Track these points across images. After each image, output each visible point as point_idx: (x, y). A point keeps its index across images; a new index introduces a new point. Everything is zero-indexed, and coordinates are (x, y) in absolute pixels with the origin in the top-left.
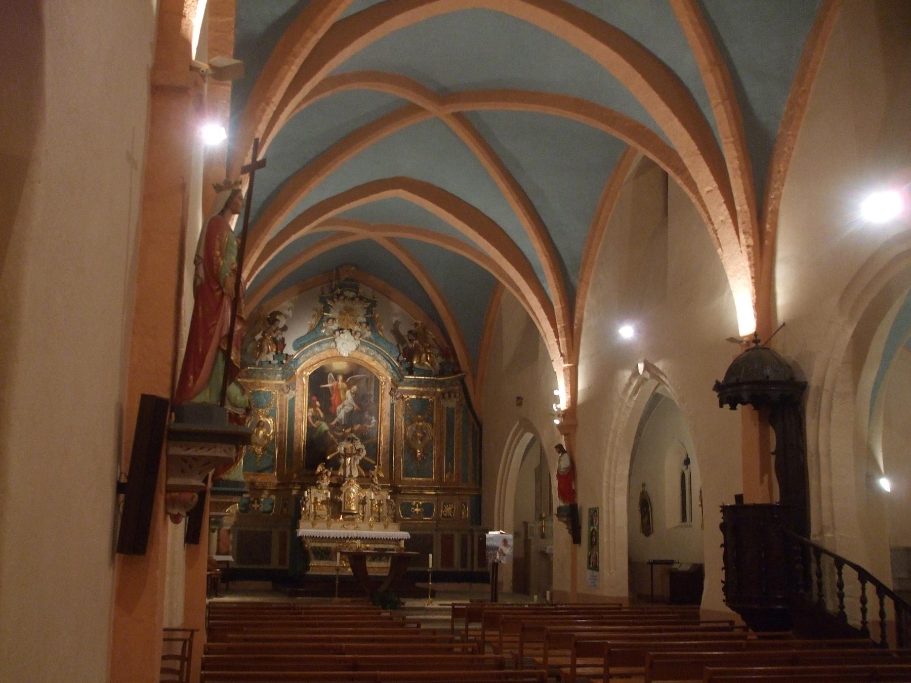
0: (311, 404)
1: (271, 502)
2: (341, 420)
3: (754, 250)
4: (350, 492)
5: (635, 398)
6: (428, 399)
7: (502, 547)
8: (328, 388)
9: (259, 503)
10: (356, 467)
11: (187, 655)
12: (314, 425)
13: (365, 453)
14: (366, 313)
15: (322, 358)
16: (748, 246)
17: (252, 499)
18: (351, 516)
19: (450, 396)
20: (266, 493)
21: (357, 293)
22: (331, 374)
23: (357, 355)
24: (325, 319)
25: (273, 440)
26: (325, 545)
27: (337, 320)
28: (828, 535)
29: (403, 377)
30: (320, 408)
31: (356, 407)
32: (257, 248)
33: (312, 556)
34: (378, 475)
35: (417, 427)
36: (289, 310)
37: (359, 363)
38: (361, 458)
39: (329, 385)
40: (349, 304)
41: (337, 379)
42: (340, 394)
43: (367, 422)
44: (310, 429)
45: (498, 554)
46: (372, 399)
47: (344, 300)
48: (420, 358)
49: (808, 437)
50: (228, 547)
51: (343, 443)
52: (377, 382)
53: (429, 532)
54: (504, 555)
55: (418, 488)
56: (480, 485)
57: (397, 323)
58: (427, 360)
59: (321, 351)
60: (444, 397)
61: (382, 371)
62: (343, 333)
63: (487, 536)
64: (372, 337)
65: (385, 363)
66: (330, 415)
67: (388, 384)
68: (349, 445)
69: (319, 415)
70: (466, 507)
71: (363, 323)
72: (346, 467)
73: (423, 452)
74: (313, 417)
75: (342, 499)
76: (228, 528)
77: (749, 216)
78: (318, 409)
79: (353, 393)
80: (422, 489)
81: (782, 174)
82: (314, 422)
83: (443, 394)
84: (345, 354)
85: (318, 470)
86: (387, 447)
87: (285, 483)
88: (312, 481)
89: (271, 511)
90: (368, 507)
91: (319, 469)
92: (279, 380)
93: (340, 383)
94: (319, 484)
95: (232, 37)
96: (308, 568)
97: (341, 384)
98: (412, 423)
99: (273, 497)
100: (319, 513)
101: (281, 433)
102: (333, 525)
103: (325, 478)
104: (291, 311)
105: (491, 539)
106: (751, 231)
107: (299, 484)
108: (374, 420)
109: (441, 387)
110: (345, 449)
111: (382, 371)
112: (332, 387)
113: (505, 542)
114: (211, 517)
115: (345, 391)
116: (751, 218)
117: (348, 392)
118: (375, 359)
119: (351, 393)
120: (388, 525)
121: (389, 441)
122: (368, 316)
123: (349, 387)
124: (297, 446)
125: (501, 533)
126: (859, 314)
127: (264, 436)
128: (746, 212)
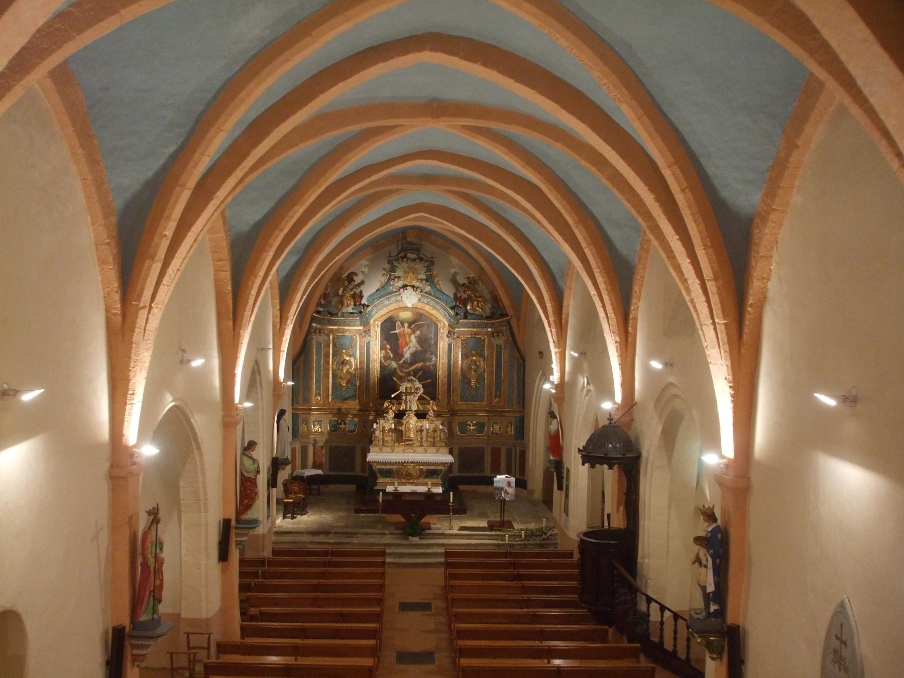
0: (383, 348)
1: (354, 423)
2: (407, 359)
3: (620, 345)
4: (409, 424)
5: (587, 398)
6: (481, 338)
7: (506, 488)
8: (396, 333)
9: (345, 424)
10: (415, 402)
11: (192, 667)
12: (386, 364)
13: (422, 390)
14: (425, 271)
15: (391, 310)
16: (616, 342)
17: (339, 421)
18: (410, 442)
19: (498, 335)
20: (350, 416)
21: (418, 255)
22: (399, 322)
23: (420, 305)
24: (392, 278)
25: (355, 374)
26: (388, 467)
27: (402, 278)
28: (646, 560)
29: (459, 321)
30: (390, 350)
31: (419, 348)
32: (305, 277)
33: (379, 475)
34: (433, 409)
35: (472, 360)
36: (365, 267)
37: (421, 312)
38: (419, 395)
39: (397, 331)
40: (412, 264)
41: (403, 326)
42: (406, 338)
43: (428, 360)
44: (382, 367)
45: (503, 493)
46: (432, 342)
47: (407, 261)
48: (473, 304)
49: (640, 490)
50: (322, 459)
51: (404, 383)
52: (437, 326)
53: (482, 446)
54: (508, 493)
55: (472, 411)
56: (524, 408)
57: (455, 274)
58: (478, 307)
59: (391, 304)
60: (493, 336)
61: (441, 317)
62: (406, 289)
63: (495, 479)
64: (431, 291)
65: (442, 311)
66: (398, 355)
67: (445, 328)
68: (409, 385)
69: (390, 356)
70: (511, 426)
71: (424, 279)
72: (407, 402)
73: (477, 382)
74: (385, 358)
75: (403, 429)
76: (322, 444)
77: (616, 321)
78: (389, 351)
79: (417, 337)
80: (475, 411)
81: (638, 293)
82: (386, 362)
83: (493, 333)
84: (409, 305)
85: (385, 406)
86: (446, 380)
87: (364, 410)
88: (381, 413)
89: (355, 430)
90: (425, 433)
91: (386, 404)
92: (358, 326)
93: (406, 329)
94: (385, 416)
95: (225, 244)
96: (376, 484)
97: (407, 330)
98: (467, 357)
99: (356, 420)
100: (386, 438)
101: (361, 369)
102: (396, 449)
103: (391, 412)
104: (367, 268)
105: (498, 481)
106: (617, 332)
107: (374, 411)
108: (434, 359)
109: (491, 327)
110: (406, 388)
111: (441, 317)
112: (400, 333)
113: (509, 484)
114: (236, 541)
115: (410, 335)
116: (618, 323)
117: (413, 336)
118: (434, 308)
119: (416, 337)
120: (439, 449)
121: (447, 375)
122: (427, 274)
123: (414, 332)
124: (373, 381)
125: (507, 477)
126: (664, 419)
127: (348, 372)
128: (613, 318)
